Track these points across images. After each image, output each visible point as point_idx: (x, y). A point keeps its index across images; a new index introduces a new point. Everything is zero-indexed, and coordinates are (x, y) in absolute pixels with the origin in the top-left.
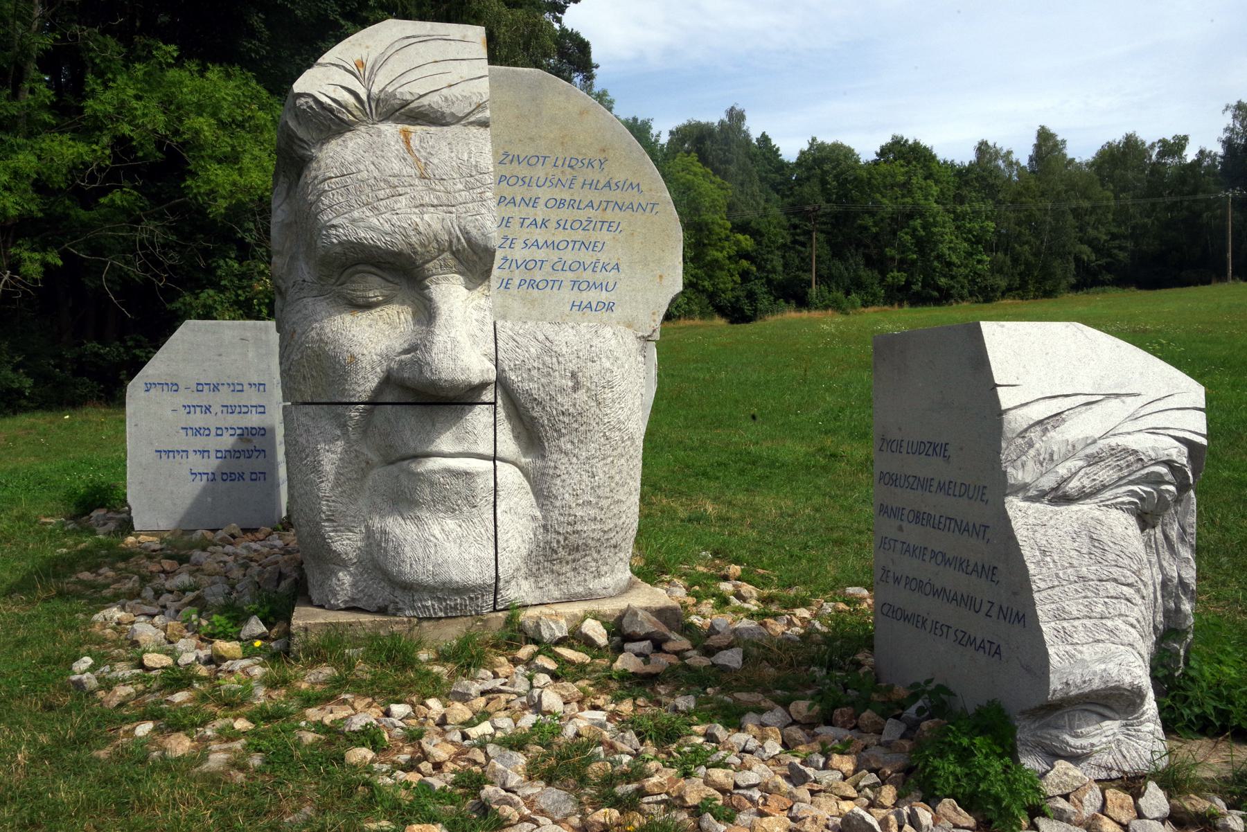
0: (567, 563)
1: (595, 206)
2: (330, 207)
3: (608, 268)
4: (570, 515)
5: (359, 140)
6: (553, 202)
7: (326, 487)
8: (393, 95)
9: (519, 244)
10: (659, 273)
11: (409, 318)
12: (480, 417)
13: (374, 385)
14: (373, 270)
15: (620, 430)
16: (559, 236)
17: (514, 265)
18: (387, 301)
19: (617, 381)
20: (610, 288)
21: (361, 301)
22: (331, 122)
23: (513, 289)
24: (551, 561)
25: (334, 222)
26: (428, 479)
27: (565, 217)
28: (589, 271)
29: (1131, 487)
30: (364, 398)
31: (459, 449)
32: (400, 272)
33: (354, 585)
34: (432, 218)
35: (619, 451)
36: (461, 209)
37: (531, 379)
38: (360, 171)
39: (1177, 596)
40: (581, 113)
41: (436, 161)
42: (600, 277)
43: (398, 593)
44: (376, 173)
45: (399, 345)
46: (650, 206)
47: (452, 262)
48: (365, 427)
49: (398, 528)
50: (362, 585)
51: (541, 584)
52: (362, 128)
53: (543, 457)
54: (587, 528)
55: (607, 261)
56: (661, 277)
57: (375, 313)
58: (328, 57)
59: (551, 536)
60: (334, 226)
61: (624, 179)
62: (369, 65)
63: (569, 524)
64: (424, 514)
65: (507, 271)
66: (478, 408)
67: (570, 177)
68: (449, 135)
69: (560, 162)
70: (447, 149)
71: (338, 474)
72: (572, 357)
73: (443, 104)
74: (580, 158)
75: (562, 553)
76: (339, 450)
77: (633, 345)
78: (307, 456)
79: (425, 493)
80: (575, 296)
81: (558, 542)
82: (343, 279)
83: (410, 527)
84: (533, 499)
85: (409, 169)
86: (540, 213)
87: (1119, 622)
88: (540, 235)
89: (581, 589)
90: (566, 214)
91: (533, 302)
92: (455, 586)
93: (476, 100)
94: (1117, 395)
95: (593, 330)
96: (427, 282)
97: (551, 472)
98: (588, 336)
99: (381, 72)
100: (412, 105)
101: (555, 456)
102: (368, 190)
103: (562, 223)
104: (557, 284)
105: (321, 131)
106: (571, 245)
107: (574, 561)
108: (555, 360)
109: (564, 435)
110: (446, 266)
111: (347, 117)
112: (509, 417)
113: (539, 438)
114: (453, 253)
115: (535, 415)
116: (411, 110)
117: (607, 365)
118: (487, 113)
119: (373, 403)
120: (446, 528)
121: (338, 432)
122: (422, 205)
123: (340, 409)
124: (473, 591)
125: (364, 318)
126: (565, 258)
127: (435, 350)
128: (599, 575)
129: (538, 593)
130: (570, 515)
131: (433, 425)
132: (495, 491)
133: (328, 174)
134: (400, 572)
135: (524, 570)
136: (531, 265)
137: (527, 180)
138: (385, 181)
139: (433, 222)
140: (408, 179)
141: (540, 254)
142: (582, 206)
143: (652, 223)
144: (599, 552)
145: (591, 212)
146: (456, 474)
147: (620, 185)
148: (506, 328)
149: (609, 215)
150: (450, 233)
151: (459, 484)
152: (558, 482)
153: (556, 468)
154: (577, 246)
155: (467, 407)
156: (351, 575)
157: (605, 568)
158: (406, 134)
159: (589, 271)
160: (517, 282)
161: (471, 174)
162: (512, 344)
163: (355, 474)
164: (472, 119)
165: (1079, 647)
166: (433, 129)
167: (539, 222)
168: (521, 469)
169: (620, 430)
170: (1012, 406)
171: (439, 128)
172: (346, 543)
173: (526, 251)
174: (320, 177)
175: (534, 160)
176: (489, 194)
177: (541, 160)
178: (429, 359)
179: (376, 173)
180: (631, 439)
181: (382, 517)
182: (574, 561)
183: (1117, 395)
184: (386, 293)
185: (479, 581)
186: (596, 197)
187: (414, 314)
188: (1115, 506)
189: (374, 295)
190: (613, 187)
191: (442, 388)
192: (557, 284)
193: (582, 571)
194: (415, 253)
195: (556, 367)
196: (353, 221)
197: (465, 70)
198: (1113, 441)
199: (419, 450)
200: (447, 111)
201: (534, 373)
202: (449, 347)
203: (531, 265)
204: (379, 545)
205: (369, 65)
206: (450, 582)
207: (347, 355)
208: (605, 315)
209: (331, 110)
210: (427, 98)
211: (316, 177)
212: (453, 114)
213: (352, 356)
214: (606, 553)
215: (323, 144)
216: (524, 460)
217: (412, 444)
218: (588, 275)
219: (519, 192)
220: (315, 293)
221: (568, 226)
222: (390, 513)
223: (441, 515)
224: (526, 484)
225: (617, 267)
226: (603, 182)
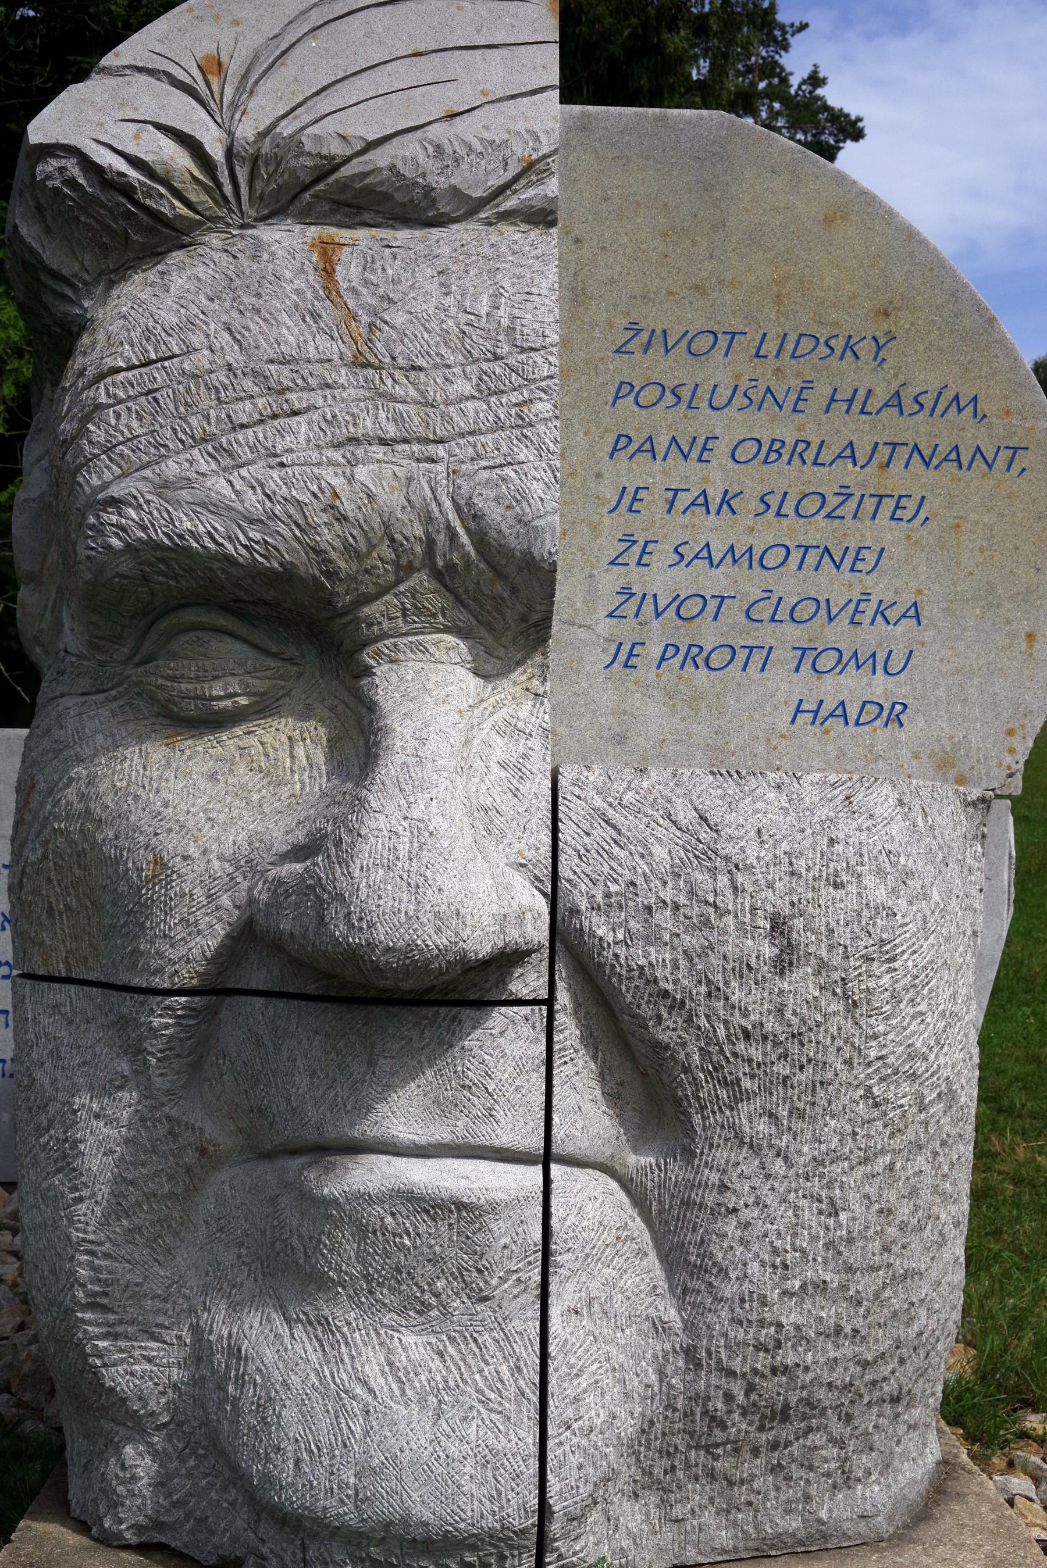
0: (756, 1452)
1: (861, 457)
2: (107, 450)
3: (892, 614)
4: (762, 1323)
5: (201, 271)
6: (751, 447)
7: (88, 1215)
8: (295, 142)
9: (662, 555)
10: (1025, 626)
11: (320, 758)
12: (505, 1044)
13: (213, 943)
14: (222, 621)
15: (913, 1077)
16: (766, 535)
17: (648, 609)
18: (263, 707)
19: (904, 940)
20: (895, 665)
21: (191, 708)
22: (131, 224)
23: (645, 671)
24: (707, 1449)
25: (115, 491)
26: (349, 1215)
28: (842, 623)
30: (187, 977)
31: (441, 1133)
32: (299, 629)
33: (160, 1484)
34: (378, 477)
35: (910, 1135)
36: (462, 449)
37: (653, 938)
38: (189, 350)
40: (828, 220)
41: (399, 318)
42: (871, 636)
43: (267, 1529)
44: (235, 355)
45: (282, 833)
46: (1004, 455)
47: (434, 600)
48: (195, 1053)
49: (273, 1344)
50: (182, 1486)
51: (678, 1511)
52: (214, 240)
53: (689, 1154)
54: (812, 1358)
56: (1030, 637)
57: (230, 740)
58: (128, 51)
59: (707, 1381)
60: (115, 502)
61: (937, 384)
62: (234, 69)
63: (759, 1347)
64: (343, 1314)
65: (631, 621)
66: (499, 1017)
67: (796, 383)
68: (445, 250)
69: (770, 347)
70: (434, 288)
71: (119, 1180)
72: (775, 873)
73: (431, 165)
74: (823, 335)
75: (739, 1425)
76: (125, 1115)
77: (949, 818)
78: (51, 1122)
79: (344, 1253)
80: (802, 686)
81: (729, 1397)
82: (147, 647)
83: (303, 1347)
84: (659, 1272)
85: (324, 343)
86: (716, 476)
88: (715, 532)
89: (794, 1523)
90: (784, 476)
91: (694, 701)
92: (419, 1533)
93: (521, 150)
95: (840, 793)
96: (367, 657)
97: (710, 1199)
98: (824, 812)
99: (268, 85)
100: (346, 171)
101: (721, 1155)
102: (207, 401)
103: (774, 501)
105: (105, 248)
106: (796, 556)
107: (774, 1446)
108: (723, 880)
109: (748, 1096)
110: (418, 610)
111: (171, 207)
112: (590, 1040)
113: (678, 1102)
114: (438, 575)
115: (664, 1037)
116: (344, 185)
117: (880, 894)
118: (552, 187)
119: (216, 988)
120: (401, 1359)
121: (124, 1067)
122: (353, 440)
123: (128, 1004)
124: (474, 1548)
125: (200, 755)
126: (779, 591)
127: (363, 858)
128: (848, 1480)
129: (669, 1534)
130: (762, 1323)
131: (372, 1063)
132: (546, 1252)
133: (110, 362)
134: (267, 1477)
135: (628, 1471)
136: (692, 608)
137: (685, 393)
138: (255, 374)
139: (381, 485)
140: (317, 369)
141: (715, 581)
142: (826, 457)
144: (849, 1418)
145: (848, 473)
147: (928, 400)
148: (587, 787)
150: (428, 519)
151: (439, 1236)
152: (731, 1227)
153: (723, 1188)
154: (812, 558)
155: (467, 1013)
156: (155, 1455)
157: (866, 1460)
158: (327, 250)
159: (842, 623)
160: (656, 652)
161: (496, 357)
162: (601, 833)
163: (170, 1179)
164: (510, 203)
166: (402, 235)
167: (715, 497)
168: (625, 1184)
169: (913, 1077)
171: (418, 233)
172: (141, 1370)
173: (680, 573)
174: (91, 372)
175: (703, 343)
176: (543, 408)
177: (723, 342)
178: (343, 883)
179: (235, 355)
180: (949, 1096)
181: (234, 1307)
182: (774, 1446)
184: (258, 685)
185: (490, 1522)
186: (863, 433)
187: (333, 745)
189: (225, 691)
190: (909, 405)
191: (376, 968)
192: (758, 657)
193: (796, 1472)
194: (332, 574)
195: (727, 900)
196: (164, 486)
199: (331, 1133)
200: (439, 182)
201: (664, 918)
202: (403, 849)
203: (692, 608)
204: (221, 1388)
205: (234, 69)
206: (405, 1522)
207: (144, 857)
208: (882, 736)
209: (126, 189)
210: (388, 148)
211: (81, 373)
212: (455, 191)
213: (159, 862)
214: (867, 1421)
215: (111, 284)
216: (634, 1161)
217: (312, 1114)
218: (838, 634)
219: (665, 423)
220: (85, 683)
221: (788, 508)
222: (255, 1300)
223: (389, 1318)
224: (638, 1226)
225: (915, 613)
226: (882, 394)
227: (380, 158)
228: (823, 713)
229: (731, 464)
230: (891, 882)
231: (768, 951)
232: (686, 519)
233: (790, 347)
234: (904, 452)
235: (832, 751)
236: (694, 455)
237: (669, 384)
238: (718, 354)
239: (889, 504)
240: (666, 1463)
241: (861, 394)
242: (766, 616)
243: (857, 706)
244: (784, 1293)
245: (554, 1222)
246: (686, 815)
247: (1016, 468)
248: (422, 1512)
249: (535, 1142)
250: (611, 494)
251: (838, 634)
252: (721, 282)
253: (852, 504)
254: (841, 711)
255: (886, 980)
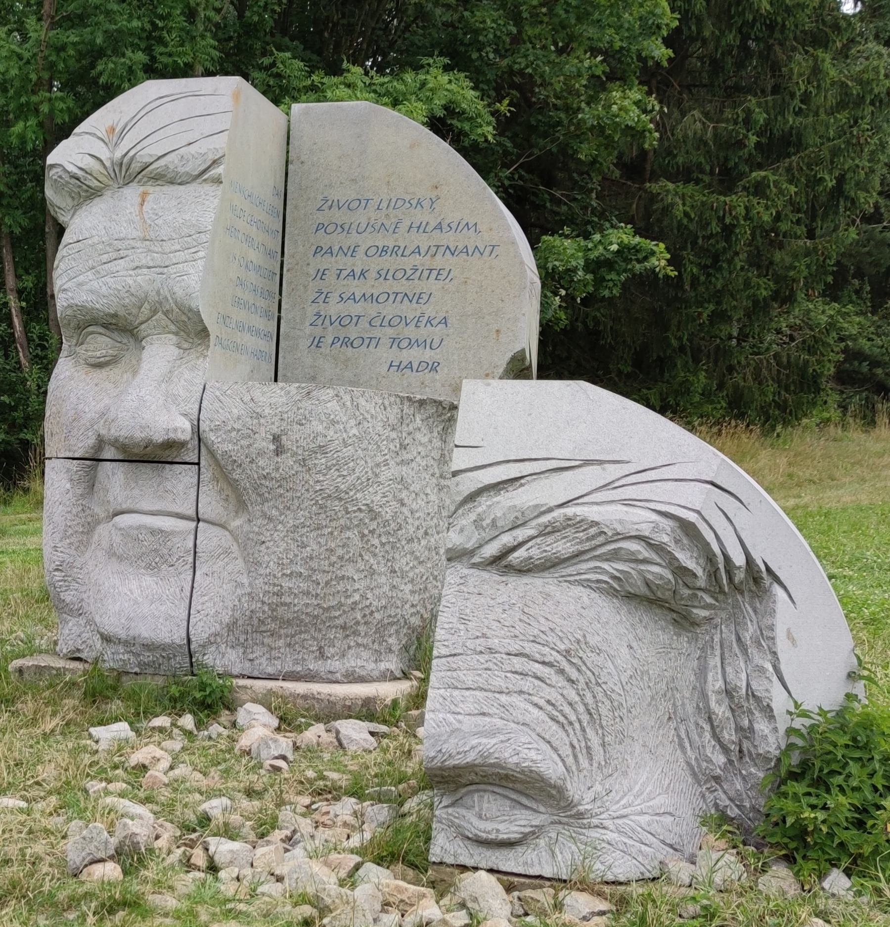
1: (423, 252)
3: (434, 322)
9: (334, 298)
17: (327, 322)
20: (435, 345)
27: (386, 266)
28: (412, 326)
29: (598, 564)
39: (750, 712)
40: (412, 146)
42: (424, 332)
46: (489, 249)
51: (251, 656)
55: (433, 315)
69: (384, 205)
87: (516, 699)
89: (299, 668)
94: (601, 462)
95: (306, 391)
104: (373, 341)
105: (73, 198)
106: (392, 297)
129: (248, 664)
132: (195, 552)
137: (346, 227)
141: (356, 309)
142: (407, 253)
143: (491, 268)
145: (417, 260)
146: (153, 532)
147: (454, 226)
149: (439, 261)
159: (412, 326)
162: (217, 405)
165: (460, 717)
167: (358, 272)
170: (463, 467)
183: (601, 462)
185: (168, 640)
186: (423, 241)
188: (579, 583)
197: (207, 126)
198: (570, 511)
200: (181, 170)
203: (346, 321)
218: (410, 332)
221: (389, 276)
227: (162, 162)
228: (402, 367)
229: (365, 258)
230: (325, 424)
231: (272, 447)
232: (345, 282)
233: (392, 204)
234: (442, 249)
235: (405, 383)
236: (349, 254)
237: (339, 223)
238: (361, 209)
239: (435, 273)
240: (244, 637)
241: (424, 224)
242: (378, 324)
243: (417, 363)
244: (284, 574)
245: (198, 542)
246: (247, 398)
247: (493, 255)
248: (145, 634)
249: (191, 512)
250: (313, 272)
251: (410, 332)
252: (363, 177)
253: (418, 273)
254: (410, 366)
255: (323, 461)
